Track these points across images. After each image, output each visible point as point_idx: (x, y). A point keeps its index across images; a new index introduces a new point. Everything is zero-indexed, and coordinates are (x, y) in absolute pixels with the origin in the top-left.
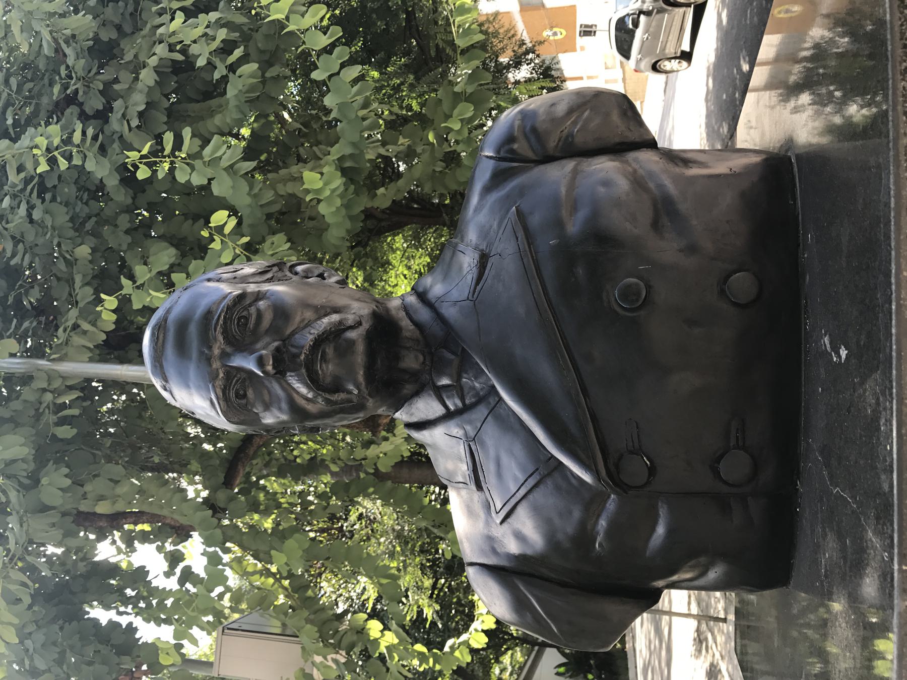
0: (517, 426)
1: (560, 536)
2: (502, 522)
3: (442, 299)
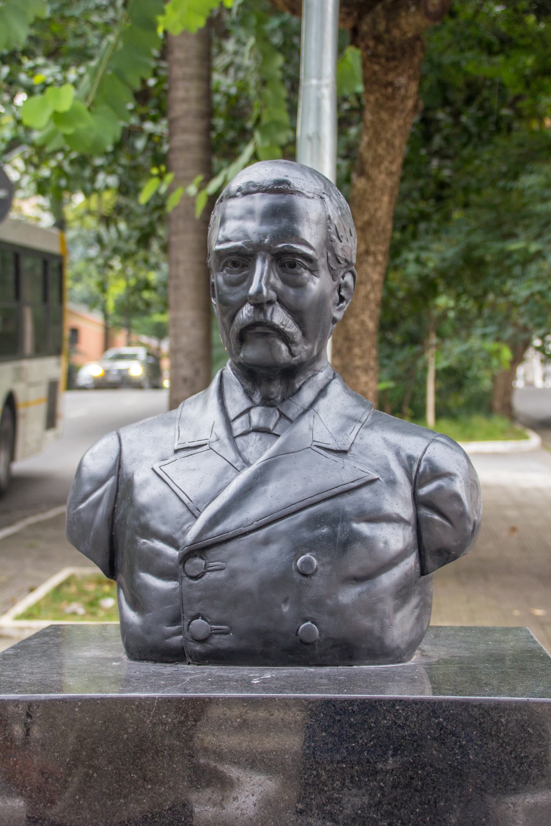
0: (220, 486)
1: (149, 515)
2: (153, 469)
3: (317, 416)
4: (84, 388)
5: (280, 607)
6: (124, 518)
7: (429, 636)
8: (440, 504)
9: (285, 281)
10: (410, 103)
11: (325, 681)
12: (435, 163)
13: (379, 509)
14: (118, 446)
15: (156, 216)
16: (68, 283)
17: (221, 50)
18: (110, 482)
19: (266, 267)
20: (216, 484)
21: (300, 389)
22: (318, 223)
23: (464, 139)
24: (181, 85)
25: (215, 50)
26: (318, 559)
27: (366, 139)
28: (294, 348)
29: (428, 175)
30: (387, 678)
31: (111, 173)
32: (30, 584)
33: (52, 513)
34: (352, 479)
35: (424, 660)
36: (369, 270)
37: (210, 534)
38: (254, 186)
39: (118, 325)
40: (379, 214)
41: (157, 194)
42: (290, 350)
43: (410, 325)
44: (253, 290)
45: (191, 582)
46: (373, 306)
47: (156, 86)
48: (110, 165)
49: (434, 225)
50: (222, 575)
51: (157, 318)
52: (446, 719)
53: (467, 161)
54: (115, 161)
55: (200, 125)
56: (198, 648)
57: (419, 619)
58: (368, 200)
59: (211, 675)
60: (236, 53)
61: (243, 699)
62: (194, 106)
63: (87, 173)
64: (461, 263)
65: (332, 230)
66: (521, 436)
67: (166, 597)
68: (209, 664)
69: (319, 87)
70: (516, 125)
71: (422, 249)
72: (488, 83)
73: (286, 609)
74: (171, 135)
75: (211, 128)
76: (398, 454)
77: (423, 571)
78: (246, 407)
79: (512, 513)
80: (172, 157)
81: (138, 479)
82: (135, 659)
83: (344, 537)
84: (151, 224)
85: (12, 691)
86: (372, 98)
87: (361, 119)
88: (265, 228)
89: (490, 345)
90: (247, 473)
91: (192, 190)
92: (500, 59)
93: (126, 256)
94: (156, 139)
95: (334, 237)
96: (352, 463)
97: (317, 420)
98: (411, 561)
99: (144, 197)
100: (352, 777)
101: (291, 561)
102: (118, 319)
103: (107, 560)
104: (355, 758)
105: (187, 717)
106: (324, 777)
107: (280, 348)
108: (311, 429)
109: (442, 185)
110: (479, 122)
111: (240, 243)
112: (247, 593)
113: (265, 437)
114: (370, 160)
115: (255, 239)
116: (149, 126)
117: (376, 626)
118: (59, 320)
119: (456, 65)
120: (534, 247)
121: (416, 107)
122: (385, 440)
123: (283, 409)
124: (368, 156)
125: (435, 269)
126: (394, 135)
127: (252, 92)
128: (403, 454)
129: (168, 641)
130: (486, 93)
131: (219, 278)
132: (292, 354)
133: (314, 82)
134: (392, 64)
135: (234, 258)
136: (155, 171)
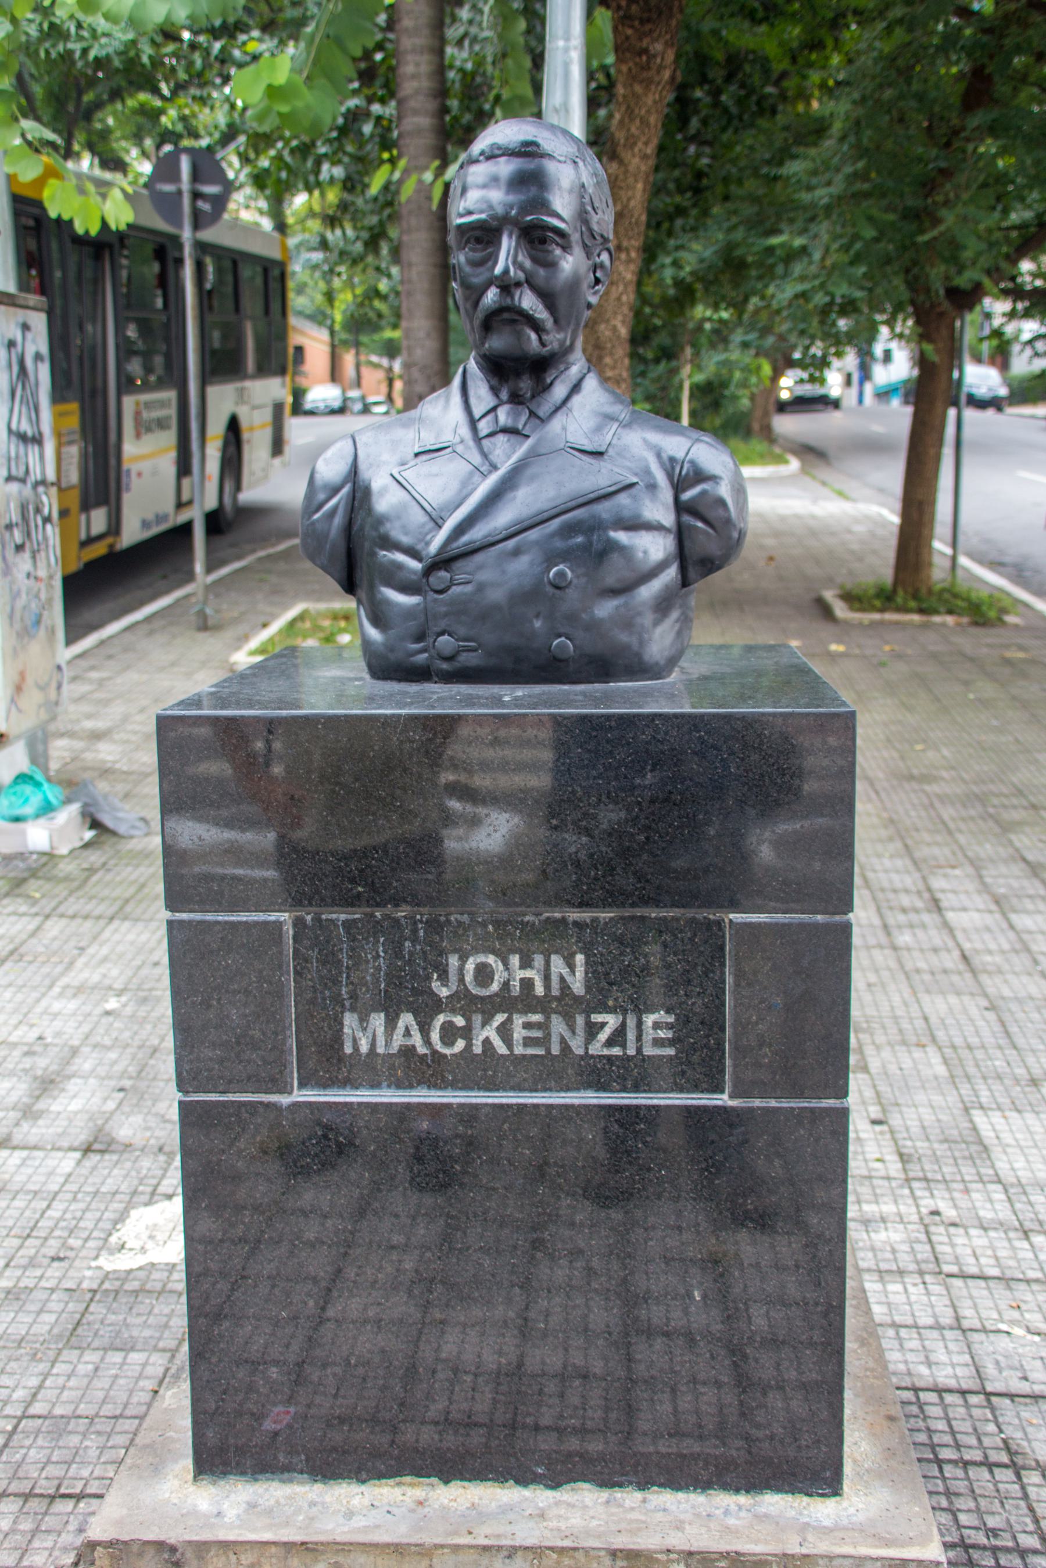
0: (465, 492)
1: (388, 525)
4: (311, 413)
5: (531, 622)
6: (362, 528)
7: (689, 654)
8: (702, 509)
9: (535, 260)
10: (667, 74)
11: (580, 698)
12: (692, 149)
13: (638, 516)
14: (352, 450)
15: (387, 212)
16: (291, 295)
17: (454, 19)
18: (346, 490)
19: (513, 244)
20: (461, 490)
21: (552, 384)
22: (571, 191)
23: (724, 122)
24: (410, 58)
25: (448, 20)
26: (572, 571)
27: (617, 116)
28: (545, 337)
29: (684, 164)
30: (646, 694)
31: (334, 163)
32: (262, 619)
33: (282, 547)
34: (609, 483)
35: (684, 677)
36: (621, 268)
37: (455, 545)
38: (499, 148)
39: (345, 343)
40: (632, 203)
41: (386, 187)
42: (540, 339)
43: (662, 339)
44: (498, 270)
45: (436, 596)
46: (625, 310)
47: (384, 60)
48: (335, 153)
49: (691, 221)
50: (468, 588)
51: (389, 334)
52: (708, 733)
53: (729, 146)
54: (341, 149)
55: (431, 105)
56: (445, 666)
57: (679, 633)
58: (621, 188)
59: (459, 693)
60: (471, 22)
61: (495, 716)
62: (426, 84)
63: (309, 164)
64: (720, 264)
65: (587, 200)
66: (780, 460)
67: (409, 613)
68: (457, 682)
69: (567, 50)
70: (780, 108)
71: (678, 248)
72: (751, 57)
73: (538, 624)
74: (400, 117)
75: (444, 110)
76: (659, 455)
77: (685, 582)
78: (492, 405)
79: (770, 542)
80: (401, 142)
81: (376, 485)
82: (378, 678)
83: (600, 547)
84: (381, 224)
85: (252, 708)
86: (624, 68)
87: (611, 97)
88: (511, 198)
89: (747, 358)
90: (494, 478)
91: (428, 176)
92: (764, 28)
93: (356, 261)
94: (385, 123)
95: (589, 208)
96: (609, 466)
97: (570, 419)
98: (672, 573)
99: (375, 187)
100: (609, 793)
101: (543, 573)
102: (344, 336)
103: (345, 574)
104: (612, 774)
105: (435, 734)
106: (580, 793)
107: (529, 338)
108: (564, 429)
109: (699, 175)
110: (740, 102)
111: (483, 216)
112: (496, 607)
113: (514, 438)
114: (622, 141)
115: (500, 210)
116: (376, 108)
117: (634, 641)
118: (281, 333)
119: (716, 33)
120: (798, 242)
121: (673, 78)
122: (645, 440)
123: (533, 407)
124: (620, 136)
125: (693, 273)
126: (648, 112)
127: (489, 68)
128: (665, 456)
129: (412, 659)
130: (747, 68)
131: (460, 258)
132: (543, 344)
133: (561, 43)
134: (648, 27)
135: (478, 233)
136: (386, 156)
